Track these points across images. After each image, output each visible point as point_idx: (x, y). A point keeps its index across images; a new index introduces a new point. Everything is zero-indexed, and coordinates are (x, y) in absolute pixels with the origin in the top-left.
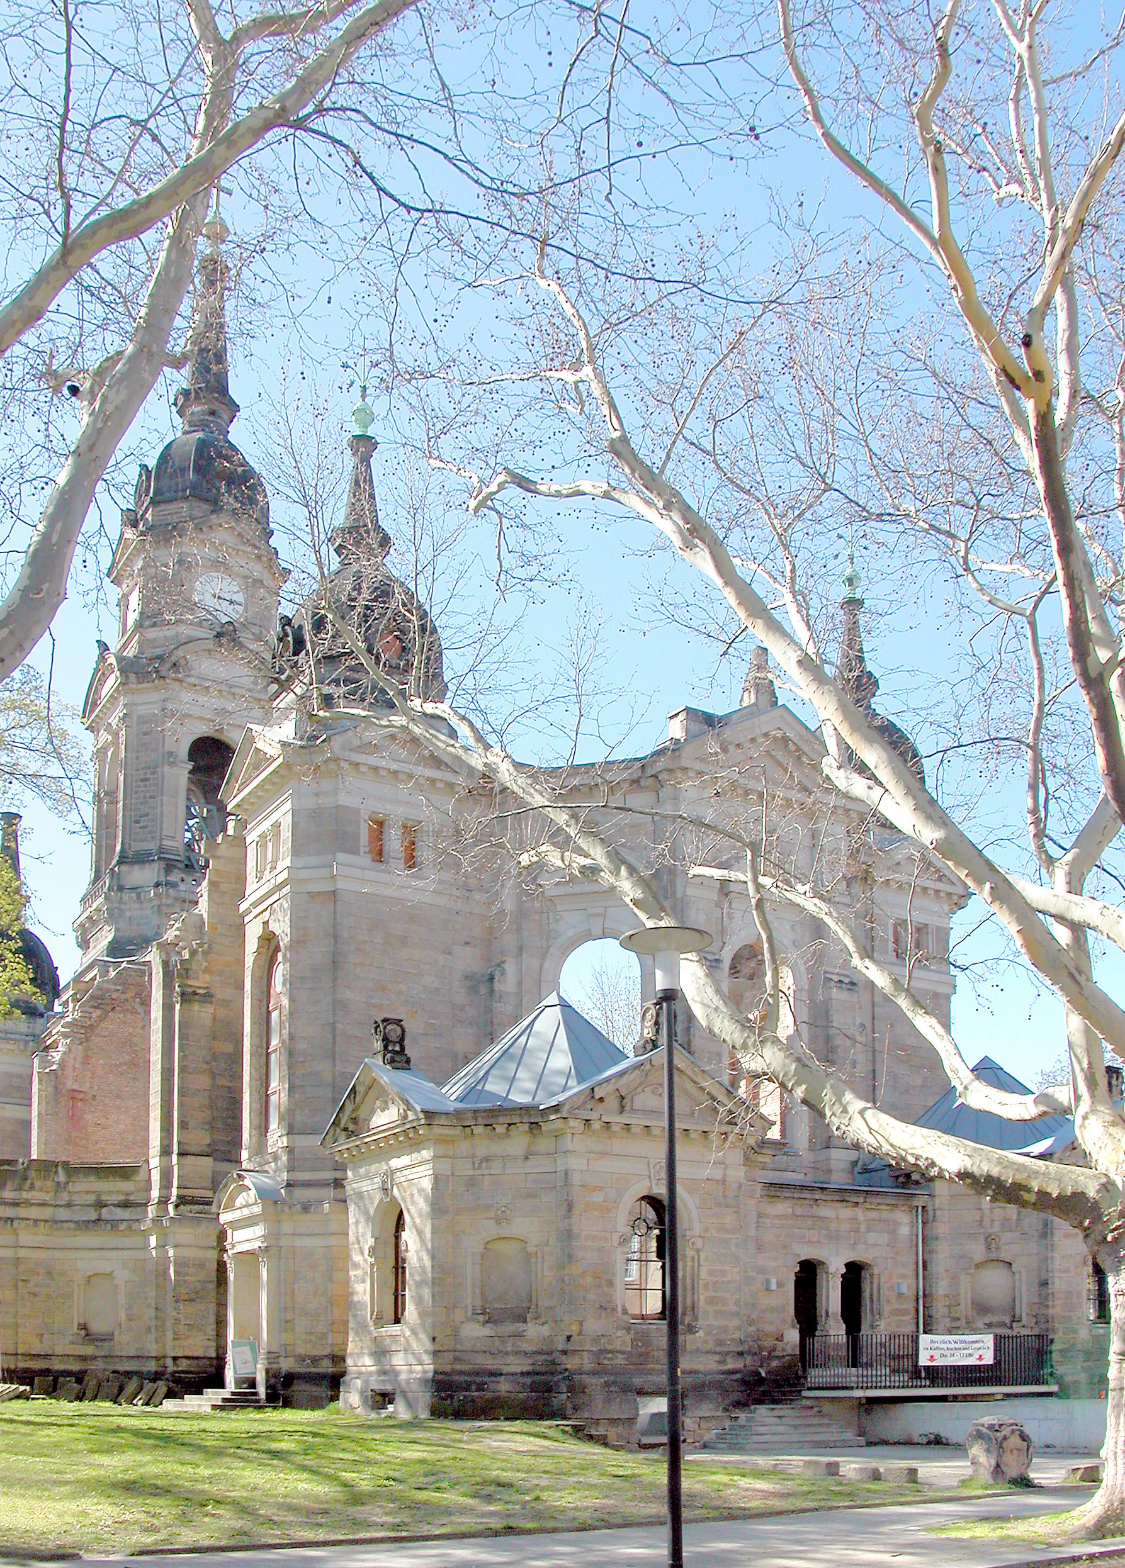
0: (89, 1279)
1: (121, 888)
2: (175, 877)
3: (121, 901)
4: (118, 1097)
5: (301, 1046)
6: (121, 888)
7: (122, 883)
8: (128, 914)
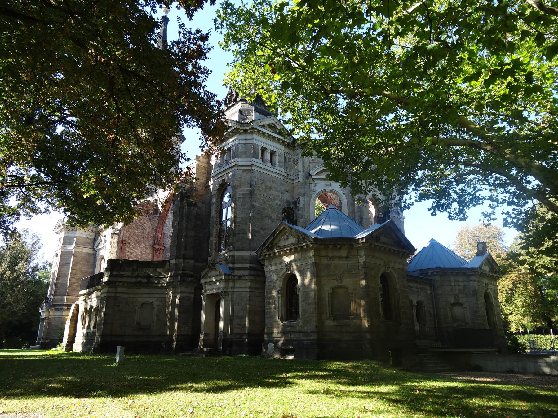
0: (142, 304)
4: (137, 243)
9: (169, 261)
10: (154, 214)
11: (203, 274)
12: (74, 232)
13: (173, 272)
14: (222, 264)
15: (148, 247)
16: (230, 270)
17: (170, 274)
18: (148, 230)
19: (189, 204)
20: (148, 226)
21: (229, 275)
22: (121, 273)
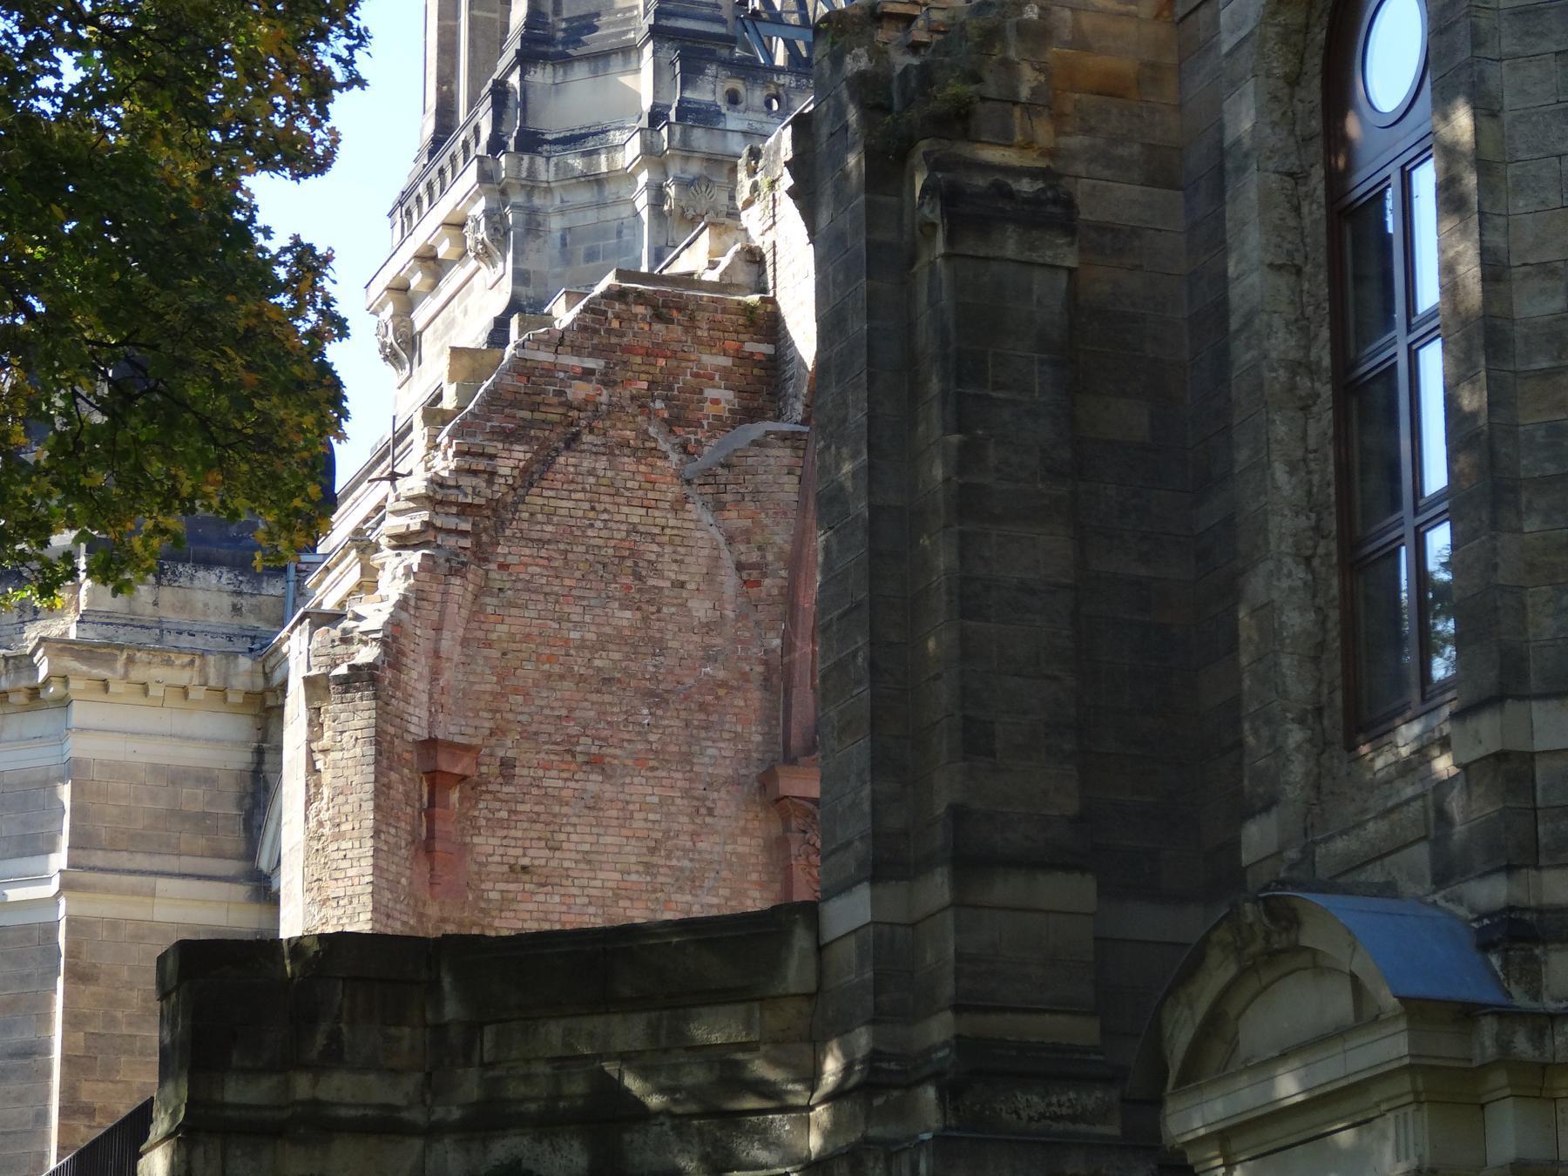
1: (530, 142)
2: (708, 91)
3: (531, 185)
4: (595, 762)
5: (1535, 305)
6: (530, 142)
7: (532, 125)
8: (555, 224)
9: (811, 912)
10: (748, 414)
11: (1180, 1039)
12: (39, 723)
13: (863, 1039)
14: (1388, 889)
15: (723, 800)
16: (1485, 945)
17: (832, 1067)
18: (701, 609)
19: (971, 209)
20: (696, 565)
21: (1467, 1014)
22: (303, 1086)
